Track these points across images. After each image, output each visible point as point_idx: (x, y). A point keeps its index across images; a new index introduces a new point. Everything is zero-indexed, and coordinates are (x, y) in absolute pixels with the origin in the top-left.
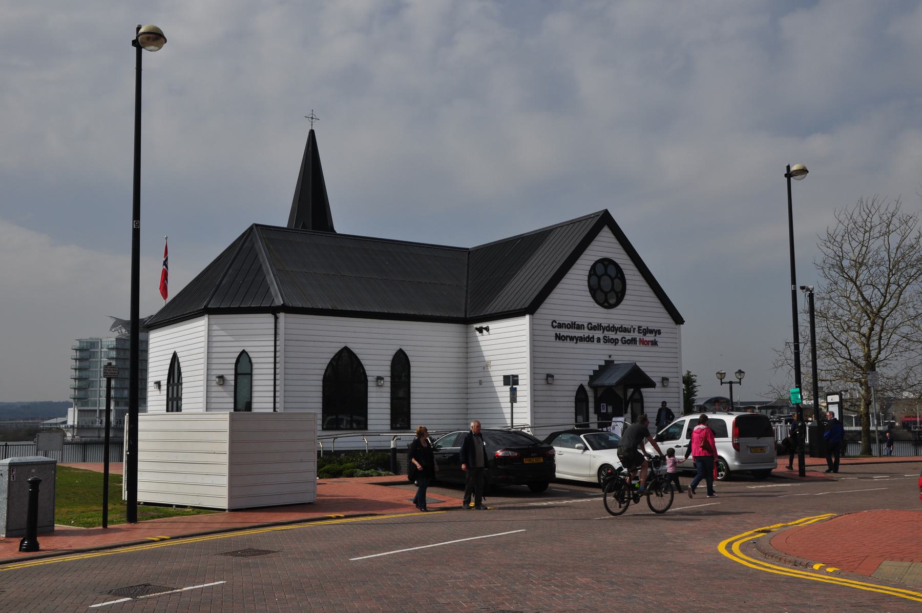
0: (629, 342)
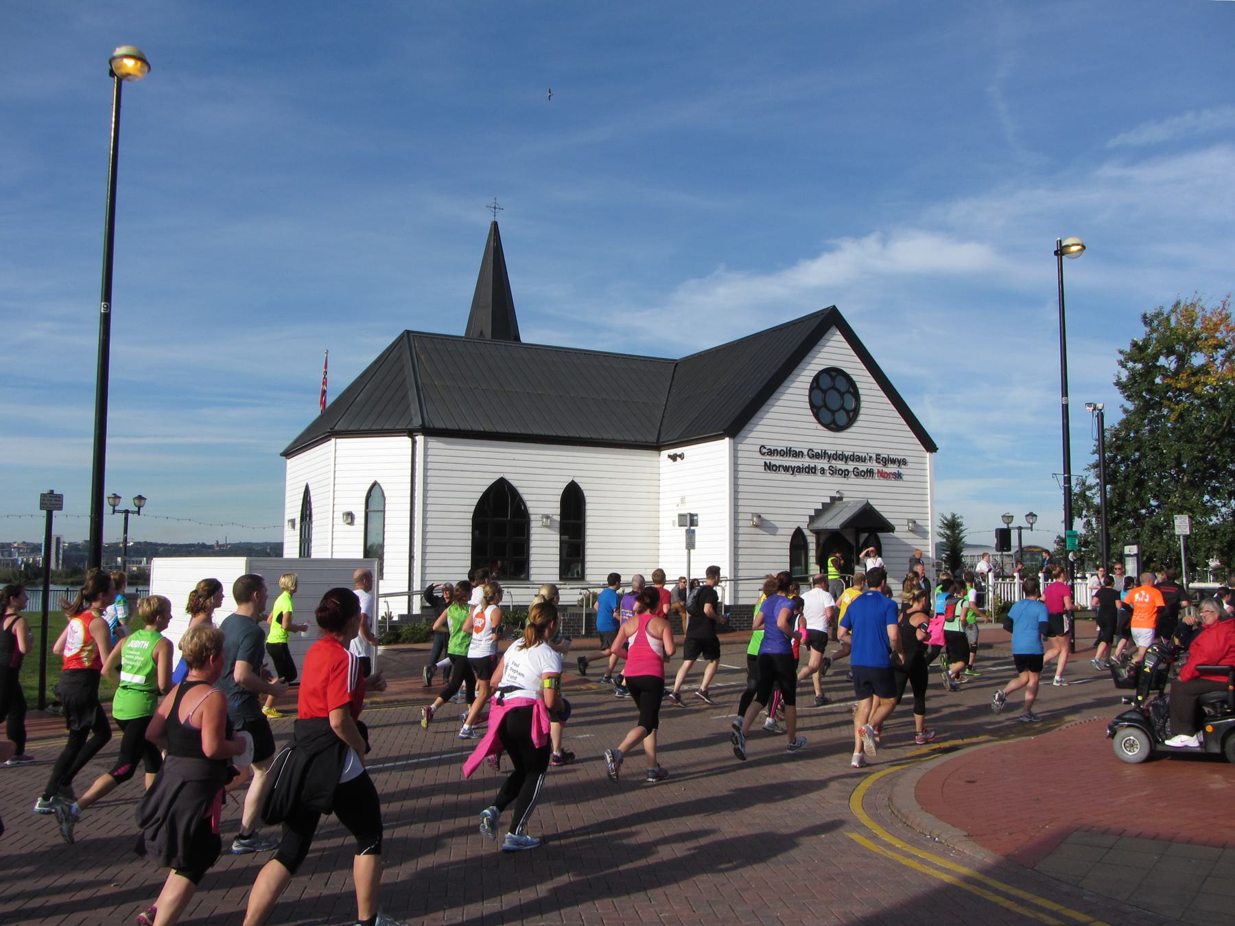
0: (863, 474)
